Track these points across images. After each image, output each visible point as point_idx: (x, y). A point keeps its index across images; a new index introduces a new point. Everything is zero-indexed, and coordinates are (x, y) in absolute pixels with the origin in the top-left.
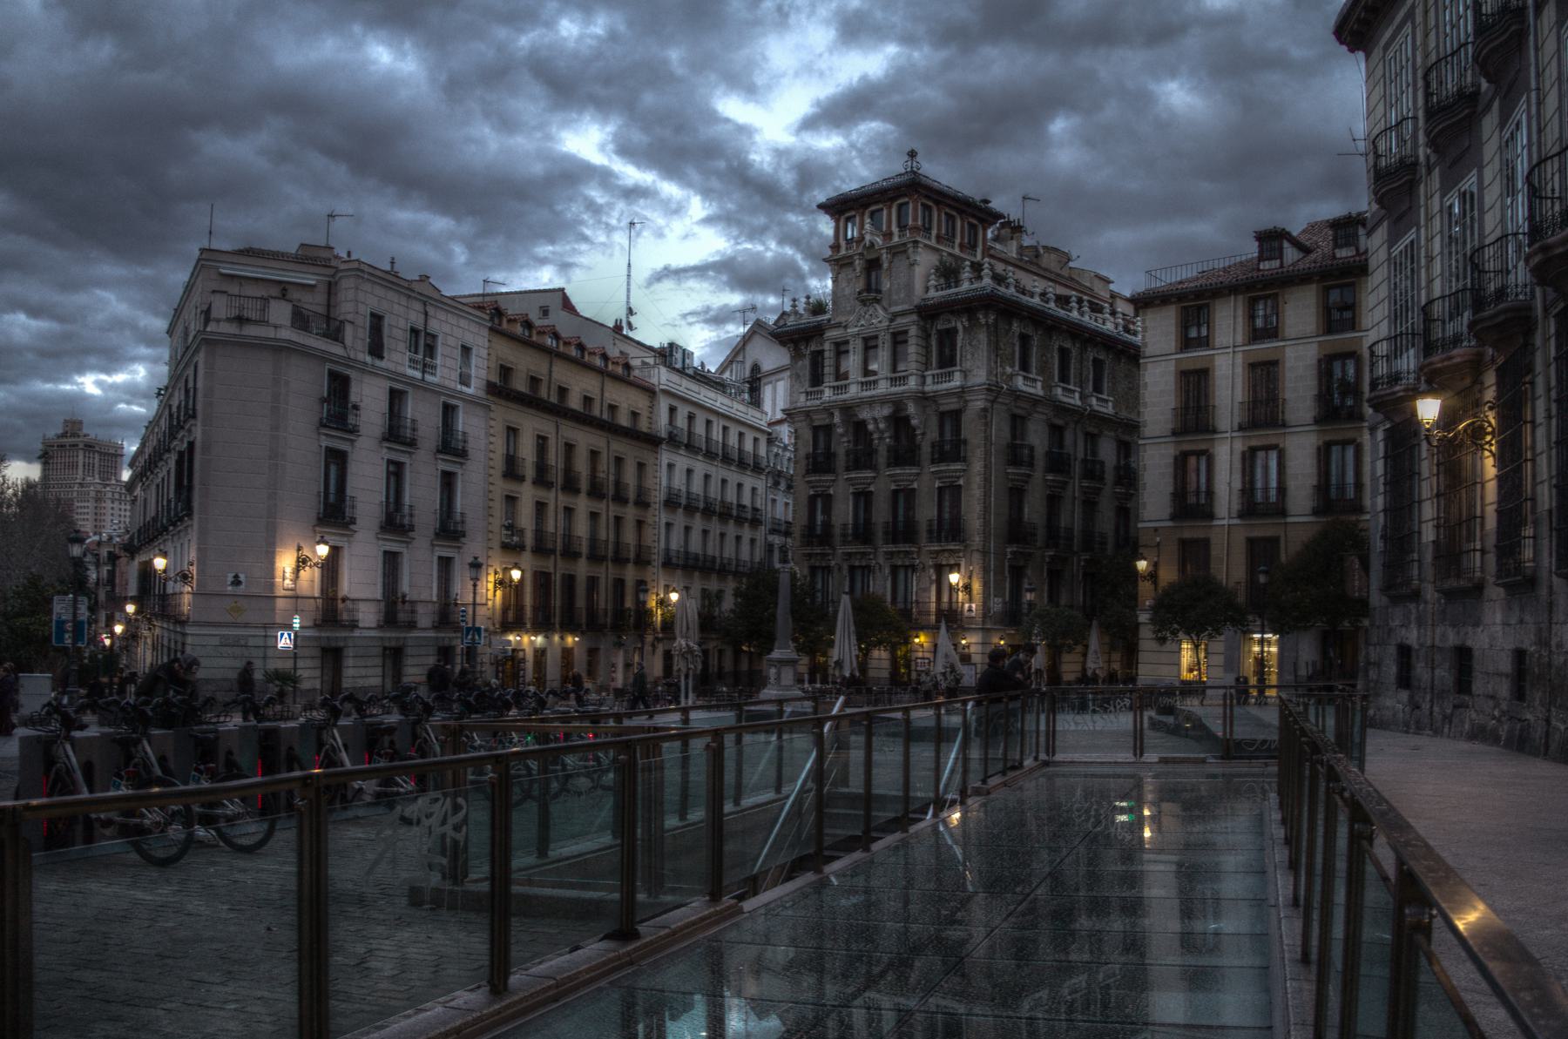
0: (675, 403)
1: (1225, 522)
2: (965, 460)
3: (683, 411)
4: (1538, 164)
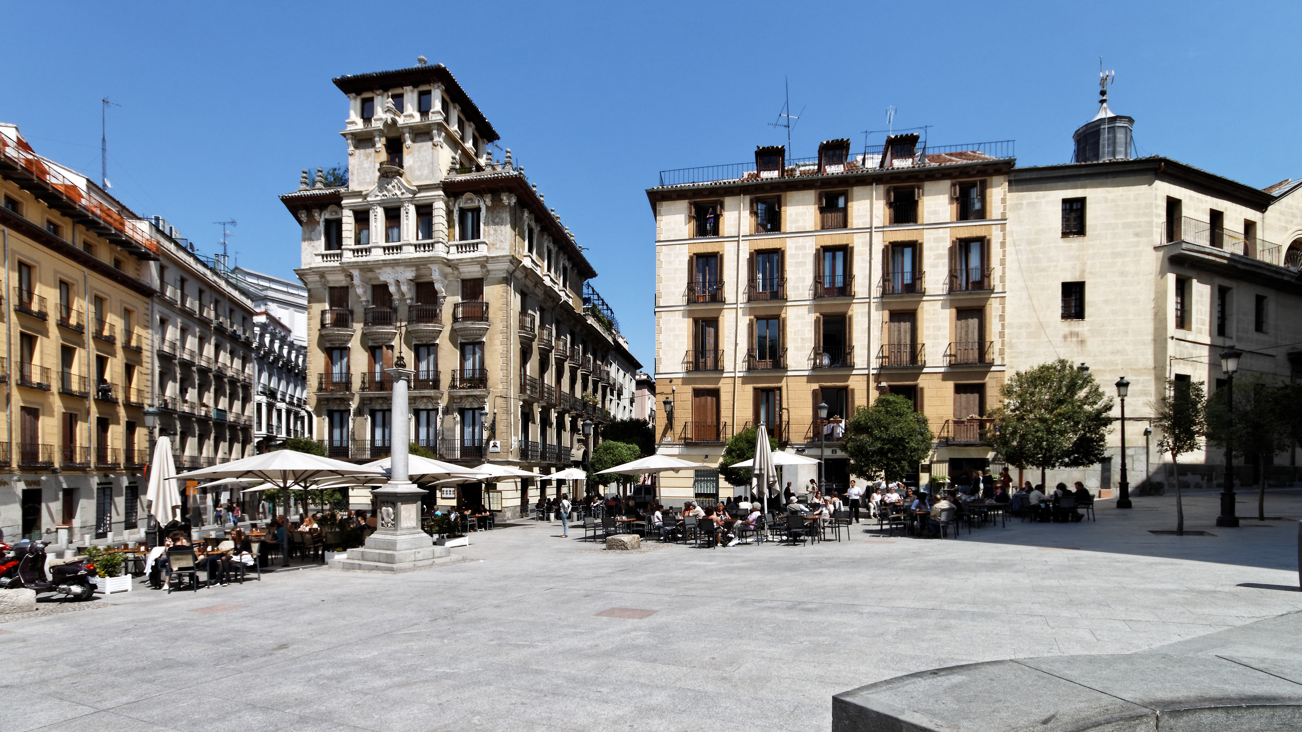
2: (487, 320)
4: (306, 284)
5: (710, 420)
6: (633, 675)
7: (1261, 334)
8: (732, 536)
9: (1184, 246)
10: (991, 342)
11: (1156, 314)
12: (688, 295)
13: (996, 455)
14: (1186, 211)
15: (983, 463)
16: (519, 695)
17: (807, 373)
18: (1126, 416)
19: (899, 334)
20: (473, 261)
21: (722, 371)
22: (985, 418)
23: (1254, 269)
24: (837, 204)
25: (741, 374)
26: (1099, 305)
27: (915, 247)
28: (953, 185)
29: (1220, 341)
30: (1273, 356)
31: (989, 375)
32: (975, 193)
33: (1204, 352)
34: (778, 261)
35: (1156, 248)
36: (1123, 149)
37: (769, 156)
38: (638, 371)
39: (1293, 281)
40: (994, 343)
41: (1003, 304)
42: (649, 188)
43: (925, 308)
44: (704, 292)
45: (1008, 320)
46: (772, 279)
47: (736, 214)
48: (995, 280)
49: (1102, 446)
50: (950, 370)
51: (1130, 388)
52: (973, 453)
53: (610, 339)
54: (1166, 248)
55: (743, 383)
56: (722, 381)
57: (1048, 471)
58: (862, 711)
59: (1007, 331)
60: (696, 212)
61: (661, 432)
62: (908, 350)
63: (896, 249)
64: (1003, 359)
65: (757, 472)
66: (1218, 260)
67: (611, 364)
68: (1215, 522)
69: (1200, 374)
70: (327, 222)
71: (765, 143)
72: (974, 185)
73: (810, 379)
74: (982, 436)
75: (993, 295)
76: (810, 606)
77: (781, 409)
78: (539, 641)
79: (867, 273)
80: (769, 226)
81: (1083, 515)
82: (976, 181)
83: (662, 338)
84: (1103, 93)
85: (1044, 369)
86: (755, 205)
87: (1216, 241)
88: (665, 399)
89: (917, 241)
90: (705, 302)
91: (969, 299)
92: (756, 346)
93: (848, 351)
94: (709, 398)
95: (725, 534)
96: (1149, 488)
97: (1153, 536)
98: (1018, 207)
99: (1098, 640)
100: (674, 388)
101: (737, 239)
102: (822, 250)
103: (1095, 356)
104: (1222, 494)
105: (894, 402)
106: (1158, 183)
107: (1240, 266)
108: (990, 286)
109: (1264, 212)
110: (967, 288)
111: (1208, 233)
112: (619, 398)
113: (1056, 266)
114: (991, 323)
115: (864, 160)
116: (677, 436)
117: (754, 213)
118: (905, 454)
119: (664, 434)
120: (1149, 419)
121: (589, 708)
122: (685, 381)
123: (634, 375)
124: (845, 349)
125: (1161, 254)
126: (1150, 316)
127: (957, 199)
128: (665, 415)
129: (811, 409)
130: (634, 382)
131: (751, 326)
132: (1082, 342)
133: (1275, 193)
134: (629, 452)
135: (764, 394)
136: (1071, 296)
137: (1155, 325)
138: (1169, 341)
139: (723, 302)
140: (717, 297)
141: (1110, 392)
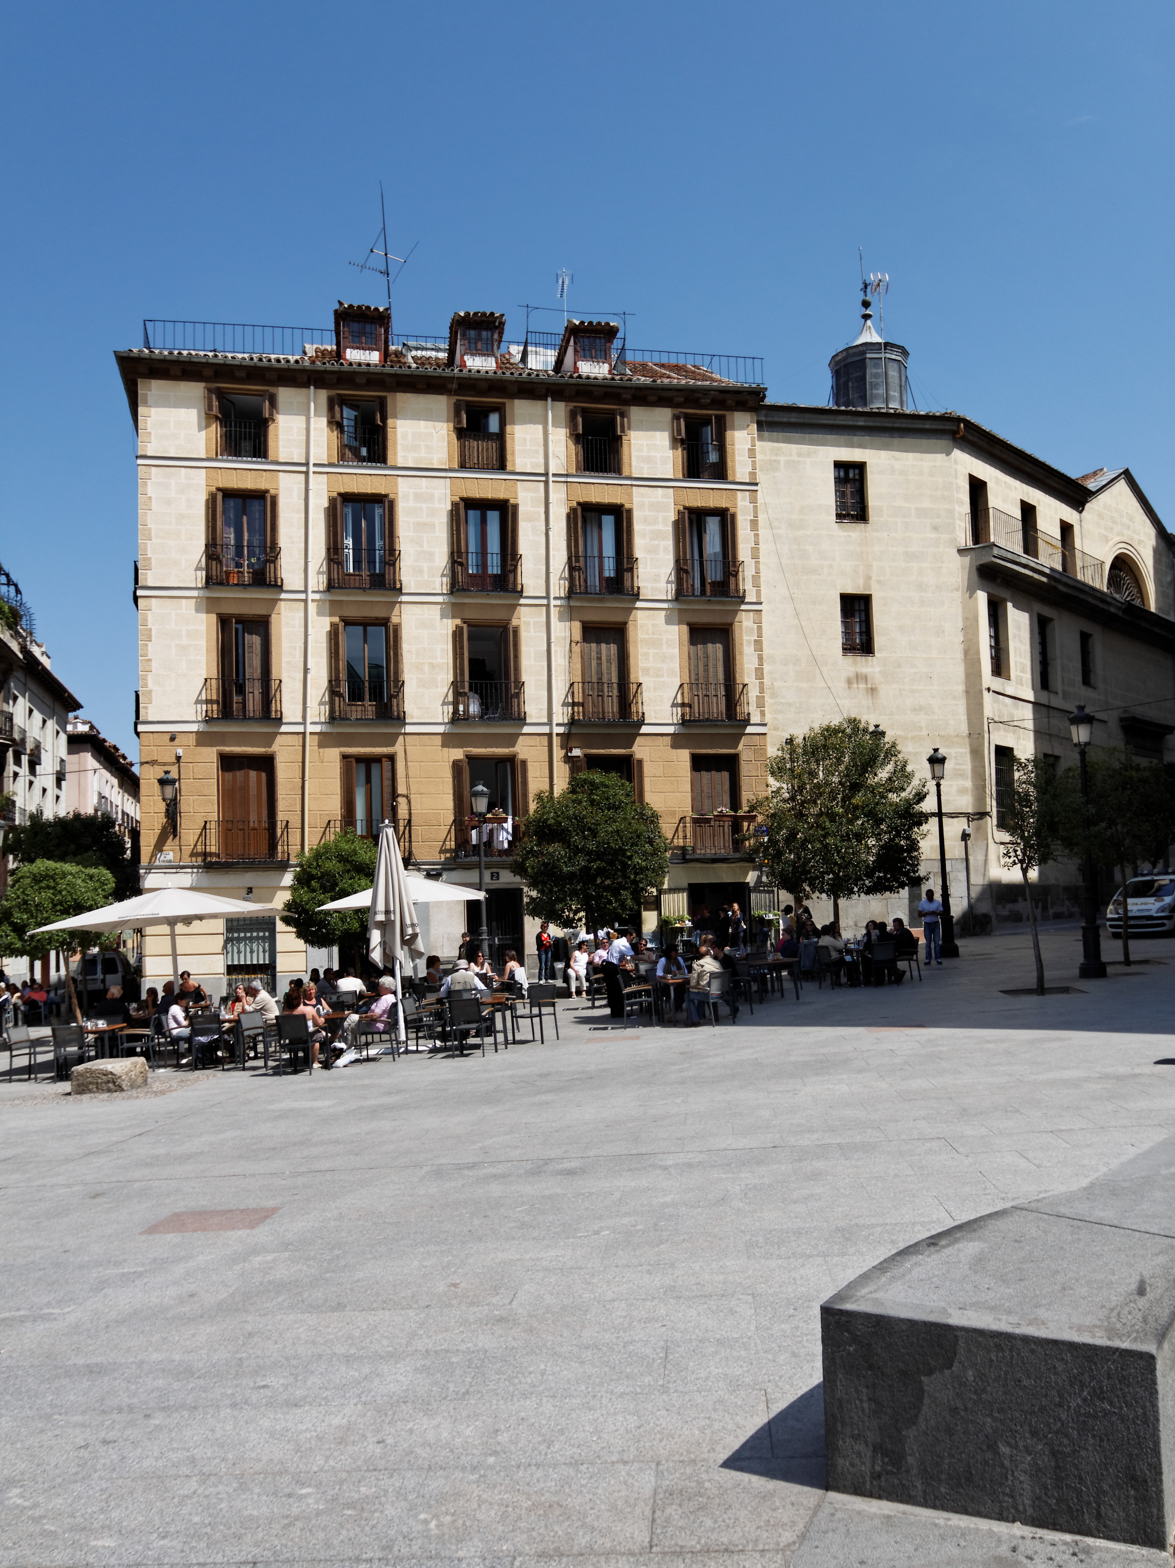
5: (256, 816)
6: (314, 1343)
7: (1090, 690)
8: (342, 1045)
9: (996, 551)
10: (745, 685)
11: (966, 652)
12: (208, 569)
13: (759, 878)
14: (994, 500)
15: (740, 892)
16: (83, 1425)
17: (441, 729)
18: (944, 810)
19: (599, 664)
21: (279, 721)
22: (740, 813)
23: (1077, 594)
24: (486, 425)
25: (318, 729)
26: (878, 632)
27: (620, 515)
28: (676, 418)
29: (1044, 698)
30: (1105, 722)
31: (744, 740)
32: (709, 432)
33: (1026, 713)
34: (382, 517)
35: (961, 551)
36: (897, 394)
37: (360, 322)
38: (71, 715)
39: (1120, 614)
40: (750, 687)
41: (759, 623)
42: (122, 348)
43: (639, 622)
44: (239, 565)
45: (766, 651)
46: (371, 550)
47: (299, 422)
48: (746, 584)
49: (915, 857)
50: (683, 730)
51: (948, 765)
52: (724, 875)
53: (15, 646)
54: (973, 552)
55: (321, 745)
56: (279, 740)
57: (842, 902)
58: (880, 1325)
59: (766, 668)
60: (221, 408)
61: (153, 841)
62: (615, 692)
63: (588, 514)
64: (763, 714)
65: (380, 917)
66: (1036, 576)
67: (15, 698)
68: (1077, 971)
69: (1025, 748)
71: (355, 299)
72: (707, 421)
73: (448, 740)
74: (737, 844)
75: (743, 607)
76: (566, 1165)
77: (394, 796)
78: (48, 1305)
79: (542, 553)
80: (364, 451)
81: (904, 972)
82: (711, 416)
83: (153, 649)
84: (866, 304)
85: (830, 732)
86: (337, 408)
87: (1031, 547)
88: (161, 775)
89: (622, 506)
90: (240, 585)
91: (709, 612)
92: (343, 676)
93: (513, 691)
94: (253, 774)
95: (325, 1045)
96: (976, 923)
97: (1009, 998)
98: (773, 466)
99: (1038, 1166)
100: (180, 751)
101: (304, 467)
102: (462, 505)
103: (892, 714)
104: (1083, 928)
105: (603, 784)
106: (957, 454)
107: (1061, 587)
108: (737, 590)
109: (1081, 512)
110: (703, 592)
111: (1020, 535)
112: (33, 771)
113: (831, 566)
114: (741, 653)
115: (525, 354)
116: (187, 850)
117: (335, 424)
118: (625, 877)
119: (159, 846)
120: (967, 815)
122: (203, 739)
123: (63, 723)
124: (507, 689)
125: (967, 560)
126: (959, 655)
127: (682, 441)
128: (162, 807)
129: (451, 797)
130: (63, 738)
131: (333, 635)
132: (873, 691)
133: (1092, 485)
134: (91, 884)
135: (362, 767)
136: (853, 616)
137: (966, 669)
138: (985, 693)
139: (278, 586)
140: (264, 578)
141: (920, 770)
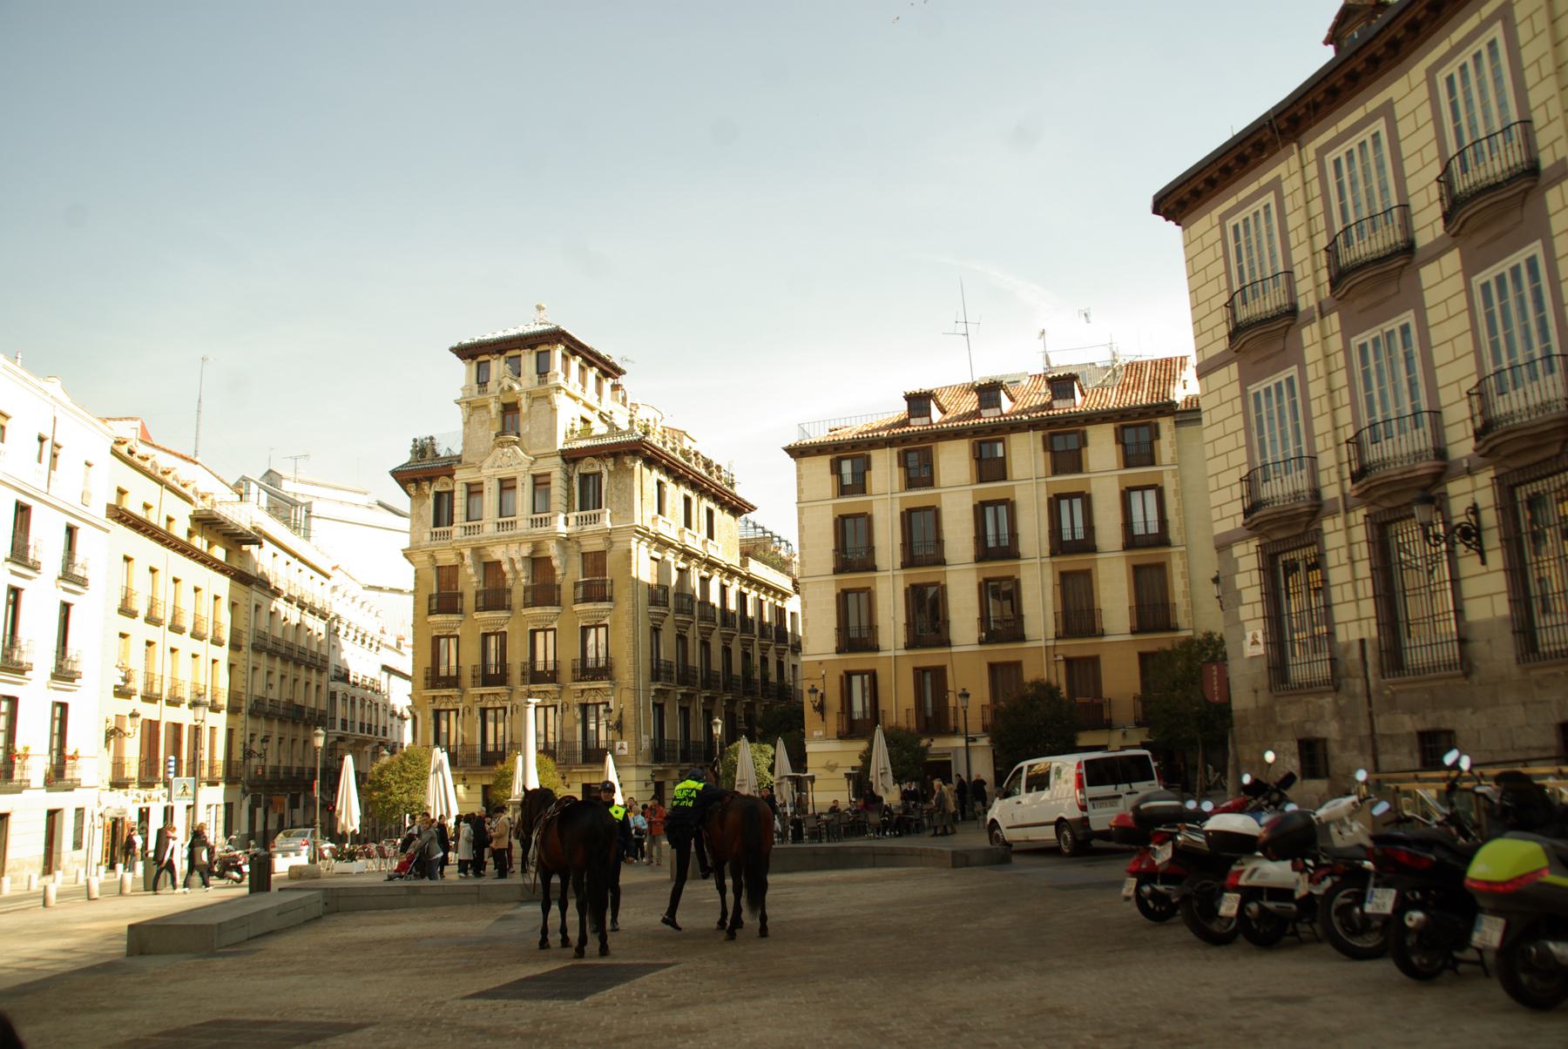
0: (74, 522)
1: (891, 654)
3: (734, 587)
18: (1353, 605)
20: (594, 534)
70: (438, 495)
71: (915, 388)
121: (725, 550)
